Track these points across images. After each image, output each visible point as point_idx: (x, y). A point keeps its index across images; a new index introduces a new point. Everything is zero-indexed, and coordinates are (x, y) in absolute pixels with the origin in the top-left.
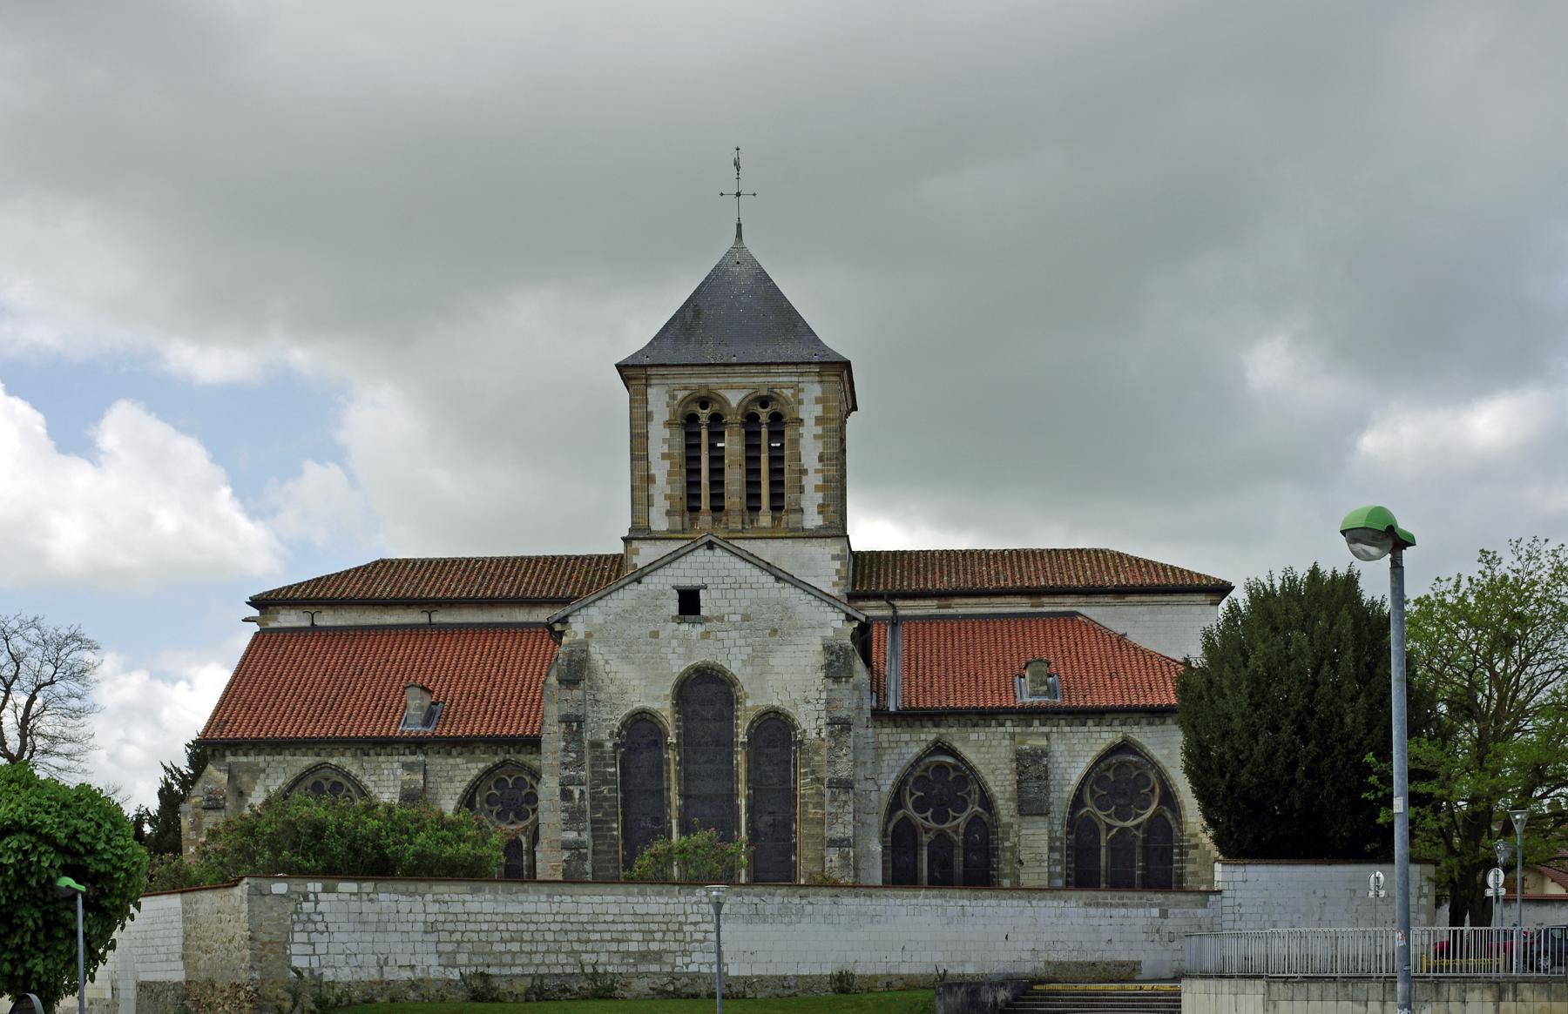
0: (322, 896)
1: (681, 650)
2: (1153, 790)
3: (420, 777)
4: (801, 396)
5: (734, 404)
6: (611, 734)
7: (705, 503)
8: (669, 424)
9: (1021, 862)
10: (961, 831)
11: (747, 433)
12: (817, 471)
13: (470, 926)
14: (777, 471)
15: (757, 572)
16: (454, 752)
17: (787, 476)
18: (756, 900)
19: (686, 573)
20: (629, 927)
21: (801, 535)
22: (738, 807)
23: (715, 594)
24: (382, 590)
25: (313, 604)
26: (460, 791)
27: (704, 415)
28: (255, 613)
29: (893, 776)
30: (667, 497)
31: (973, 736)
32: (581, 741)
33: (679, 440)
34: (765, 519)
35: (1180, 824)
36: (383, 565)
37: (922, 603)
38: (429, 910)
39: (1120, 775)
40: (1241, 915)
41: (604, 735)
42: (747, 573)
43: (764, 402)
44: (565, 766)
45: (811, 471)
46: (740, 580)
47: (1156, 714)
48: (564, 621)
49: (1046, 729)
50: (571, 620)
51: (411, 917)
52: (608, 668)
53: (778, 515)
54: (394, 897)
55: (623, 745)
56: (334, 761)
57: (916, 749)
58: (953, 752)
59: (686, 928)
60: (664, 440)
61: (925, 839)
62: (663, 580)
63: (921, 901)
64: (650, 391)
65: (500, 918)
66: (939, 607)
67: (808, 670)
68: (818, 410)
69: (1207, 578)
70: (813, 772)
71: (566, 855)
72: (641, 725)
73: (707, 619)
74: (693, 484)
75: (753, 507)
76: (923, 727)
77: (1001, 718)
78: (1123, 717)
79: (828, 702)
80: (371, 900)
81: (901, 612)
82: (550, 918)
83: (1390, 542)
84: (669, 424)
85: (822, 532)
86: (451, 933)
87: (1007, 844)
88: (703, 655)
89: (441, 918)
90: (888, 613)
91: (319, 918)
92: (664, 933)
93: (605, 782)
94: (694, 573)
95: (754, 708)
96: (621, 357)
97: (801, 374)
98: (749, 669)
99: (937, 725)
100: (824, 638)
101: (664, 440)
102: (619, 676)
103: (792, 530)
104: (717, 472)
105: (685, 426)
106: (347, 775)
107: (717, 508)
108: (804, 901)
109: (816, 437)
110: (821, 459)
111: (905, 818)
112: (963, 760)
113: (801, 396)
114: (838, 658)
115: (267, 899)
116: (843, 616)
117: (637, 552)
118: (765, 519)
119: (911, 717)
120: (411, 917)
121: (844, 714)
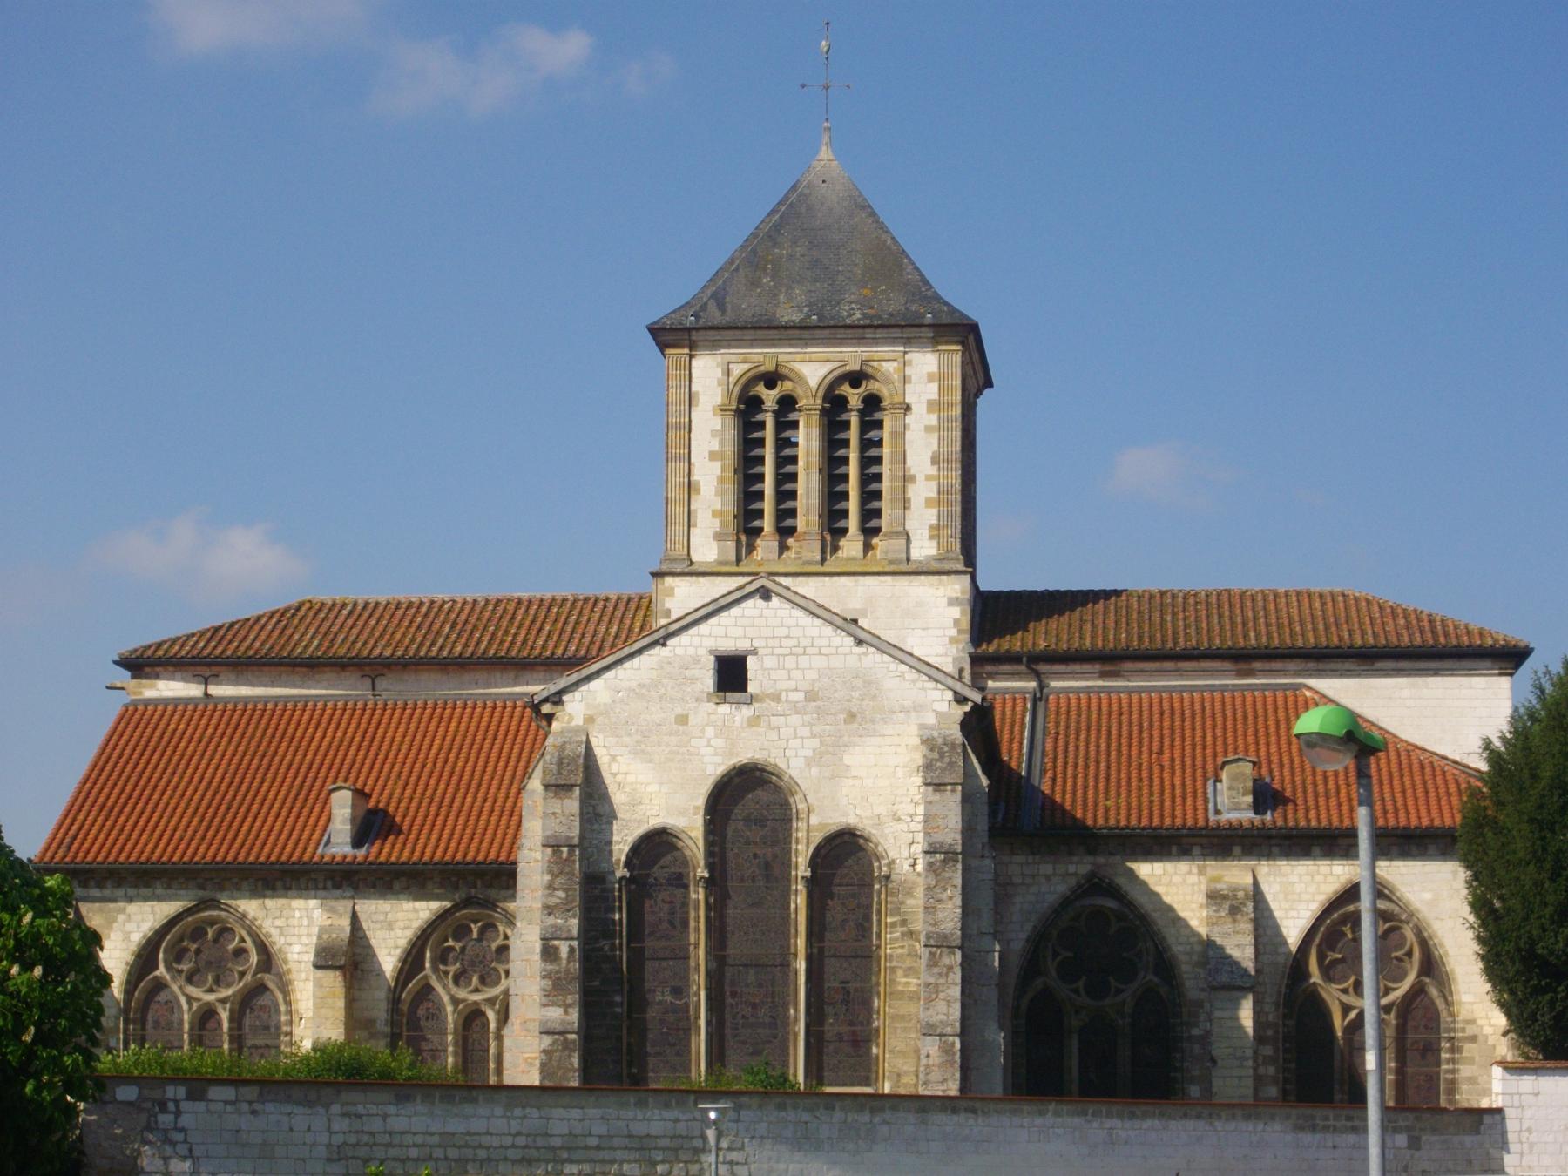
0: (185, 1106)
1: (719, 742)
2: (1409, 954)
9: (1213, 1061)
12: (928, 478)
13: (392, 1152)
14: (870, 479)
15: (829, 630)
18: (806, 1117)
19: (725, 633)
21: (908, 569)
25: (209, 665)
29: (1029, 927)
30: (715, 514)
35: (1449, 1004)
38: (336, 1127)
40: (1531, 1145)
42: (815, 632)
45: (920, 478)
46: (804, 642)
48: (557, 699)
51: (309, 1138)
52: (615, 768)
54: (288, 1108)
57: (1061, 888)
60: (714, 434)
62: (696, 640)
64: (694, 362)
65: (435, 1140)
67: (900, 772)
70: (904, 923)
76: (1071, 854)
79: (927, 819)
80: (254, 1112)
82: (508, 1141)
83: (1354, 748)
85: (935, 566)
86: (366, 1161)
87: (1196, 1032)
89: (352, 1139)
91: (179, 1137)
94: (738, 632)
95: (822, 826)
96: (656, 314)
98: (815, 770)
100: (922, 727)
101: (714, 434)
102: (631, 778)
103: (891, 562)
104: (786, 478)
109: (928, 429)
114: (942, 755)
115: (109, 1108)
116: (949, 695)
117: (670, 592)
118: (851, 545)
120: (309, 1138)
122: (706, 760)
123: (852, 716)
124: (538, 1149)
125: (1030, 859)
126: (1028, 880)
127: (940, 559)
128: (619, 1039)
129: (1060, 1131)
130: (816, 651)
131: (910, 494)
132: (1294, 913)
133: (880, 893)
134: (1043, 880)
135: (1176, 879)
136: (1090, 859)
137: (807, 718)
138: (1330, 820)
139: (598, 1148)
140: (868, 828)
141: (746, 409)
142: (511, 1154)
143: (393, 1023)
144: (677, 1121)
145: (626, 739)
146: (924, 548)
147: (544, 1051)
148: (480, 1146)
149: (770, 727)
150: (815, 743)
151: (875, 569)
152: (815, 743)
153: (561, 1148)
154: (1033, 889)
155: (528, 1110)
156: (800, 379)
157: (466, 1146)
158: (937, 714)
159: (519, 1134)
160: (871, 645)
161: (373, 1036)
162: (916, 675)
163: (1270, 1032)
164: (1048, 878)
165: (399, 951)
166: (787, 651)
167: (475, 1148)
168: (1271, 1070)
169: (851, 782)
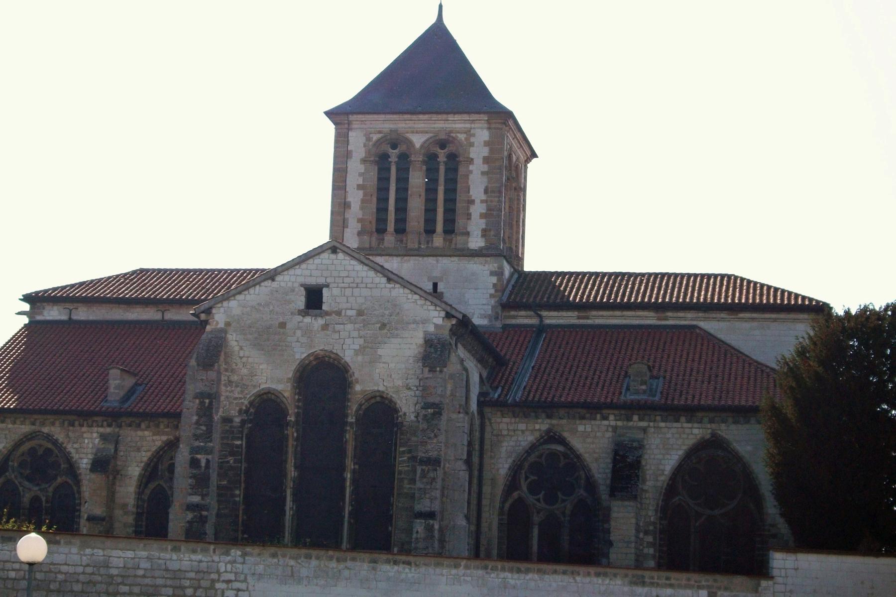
1: (304, 340)
3: (112, 447)
4: (472, 140)
5: (418, 146)
6: (240, 411)
7: (391, 227)
8: (364, 161)
10: (568, 512)
11: (428, 170)
12: (482, 202)
15: (372, 274)
16: (143, 426)
17: (460, 205)
18: (292, 563)
20: (160, 582)
22: (344, 480)
23: (336, 291)
24: (128, 293)
26: (145, 459)
27: (394, 154)
28: (26, 307)
29: (510, 461)
30: (359, 220)
31: (581, 428)
32: (210, 417)
33: (374, 174)
34: (438, 241)
36: (142, 273)
37: (564, 314)
39: (708, 466)
41: (234, 413)
42: (364, 274)
43: (443, 145)
44: (197, 437)
45: (477, 201)
46: (358, 280)
47: (743, 413)
49: (643, 424)
50: (214, 311)
53: (449, 237)
55: (251, 421)
56: (45, 430)
58: (562, 441)
59: (218, 586)
61: (536, 519)
63: (461, 571)
64: (350, 134)
66: (579, 318)
68: (485, 152)
69: (811, 300)
70: (410, 452)
71: (190, 516)
72: (266, 407)
73: (327, 313)
74: (382, 210)
75: (430, 231)
76: (537, 417)
77: (605, 412)
78: (712, 415)
81: (548, 321)
82: (80, 569)
84: (364, 161)
88: (322, 344)
90: (534, 321)
92: (196, 589)
93: (232, 454)
95: (363, 391)
97: (473, 121)
98: (360, 358)
99: (549, 417)
100: (426, 333)
101: (360, 175)
103: (459, 250)
105: (377, 163)
106: (55, 442)
107: (401, 230)
108: (342, 566)
109: (483, 173)
110: (486, 191)
111: (520, 500)
112: (571, 449)
113: (472, 140)
116: (443, 314)
118: (438, 241)
119: (527, 408)
121: (437, 400)
122: (295, 350)
123: (383, 326)
124: (101, 575)
125: (513, 420)
126: (512, 433)
127: (486, 248)
128: (237, 516)
129: (469, 579)
130: (364, 285)
131: (471, 211)
132: (669, 457)
133: (396, 433)
134: (520, 433)
135: (598, 434)
136: (549, 421)
137: (357, 326)
138: (505, 354)
139: (144, 576)
140: (391, 394)
141: (381, 161)
142: (82, 578)
143: (138, 507)
144: (201, 561)
145: (250, 337)
146: (476, 242)
147: (188, 522)
148: (60, 572)
149: (334, 331)
150: (361, 341)
151: (448, 254)
152: (361, 341)
153: (117, 575)
154: (514, 439)
155: (96, 551)
156: (410, 143)
157: (50, 571)
158: (436, 326)
159: (88, 565)
160: (397, 282)
161: (126, 513)
162: (423, 302)
163: (651, 528)
164: (523, 431)
165: (143, 465)
166: (347, 285)
167: (56, 573)
168: (651, 551)
169: (382, 365)
